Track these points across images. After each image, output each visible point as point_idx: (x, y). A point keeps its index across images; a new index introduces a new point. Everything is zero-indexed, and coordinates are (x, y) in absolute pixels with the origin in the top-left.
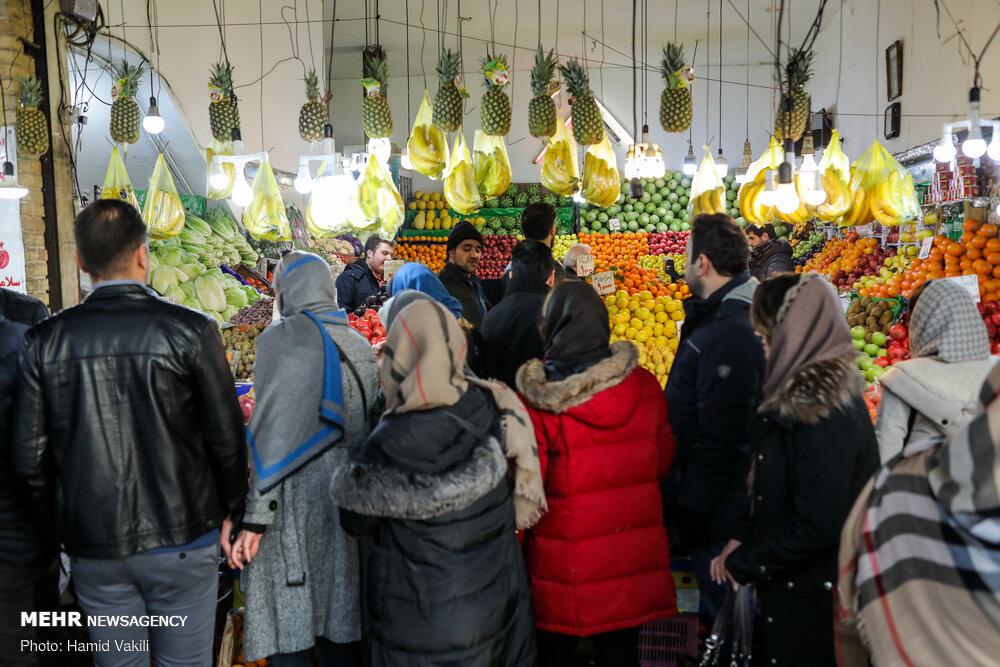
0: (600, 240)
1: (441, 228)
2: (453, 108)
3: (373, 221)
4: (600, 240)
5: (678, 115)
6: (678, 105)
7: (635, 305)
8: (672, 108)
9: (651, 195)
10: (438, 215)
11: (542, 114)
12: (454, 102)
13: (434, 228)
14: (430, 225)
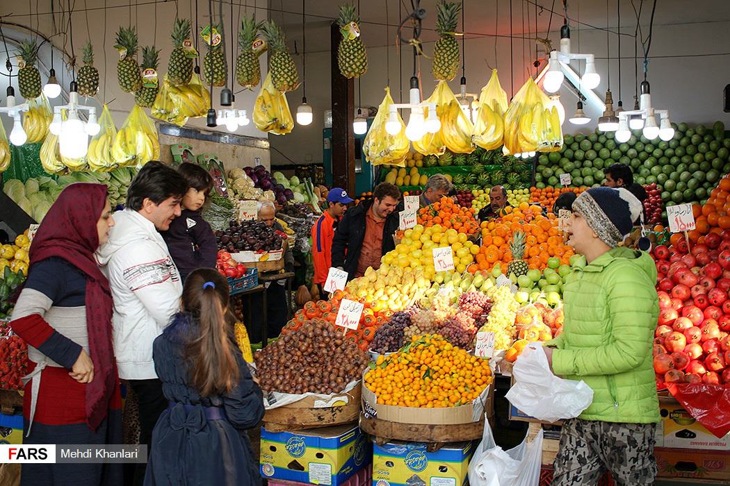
0: (550, 194)
1: (410, 185)
2: (181, 71)
3: (130, 158)
4: (550, 194)
5: (348, 62)
6: (352, 57)
7: (425, 238)
8: (348, 55)
9: (611, 151)
10: (409, 174)
11: (243, 67)
12: (185, 63)
13: (404, 185)
14: (400, 182)
